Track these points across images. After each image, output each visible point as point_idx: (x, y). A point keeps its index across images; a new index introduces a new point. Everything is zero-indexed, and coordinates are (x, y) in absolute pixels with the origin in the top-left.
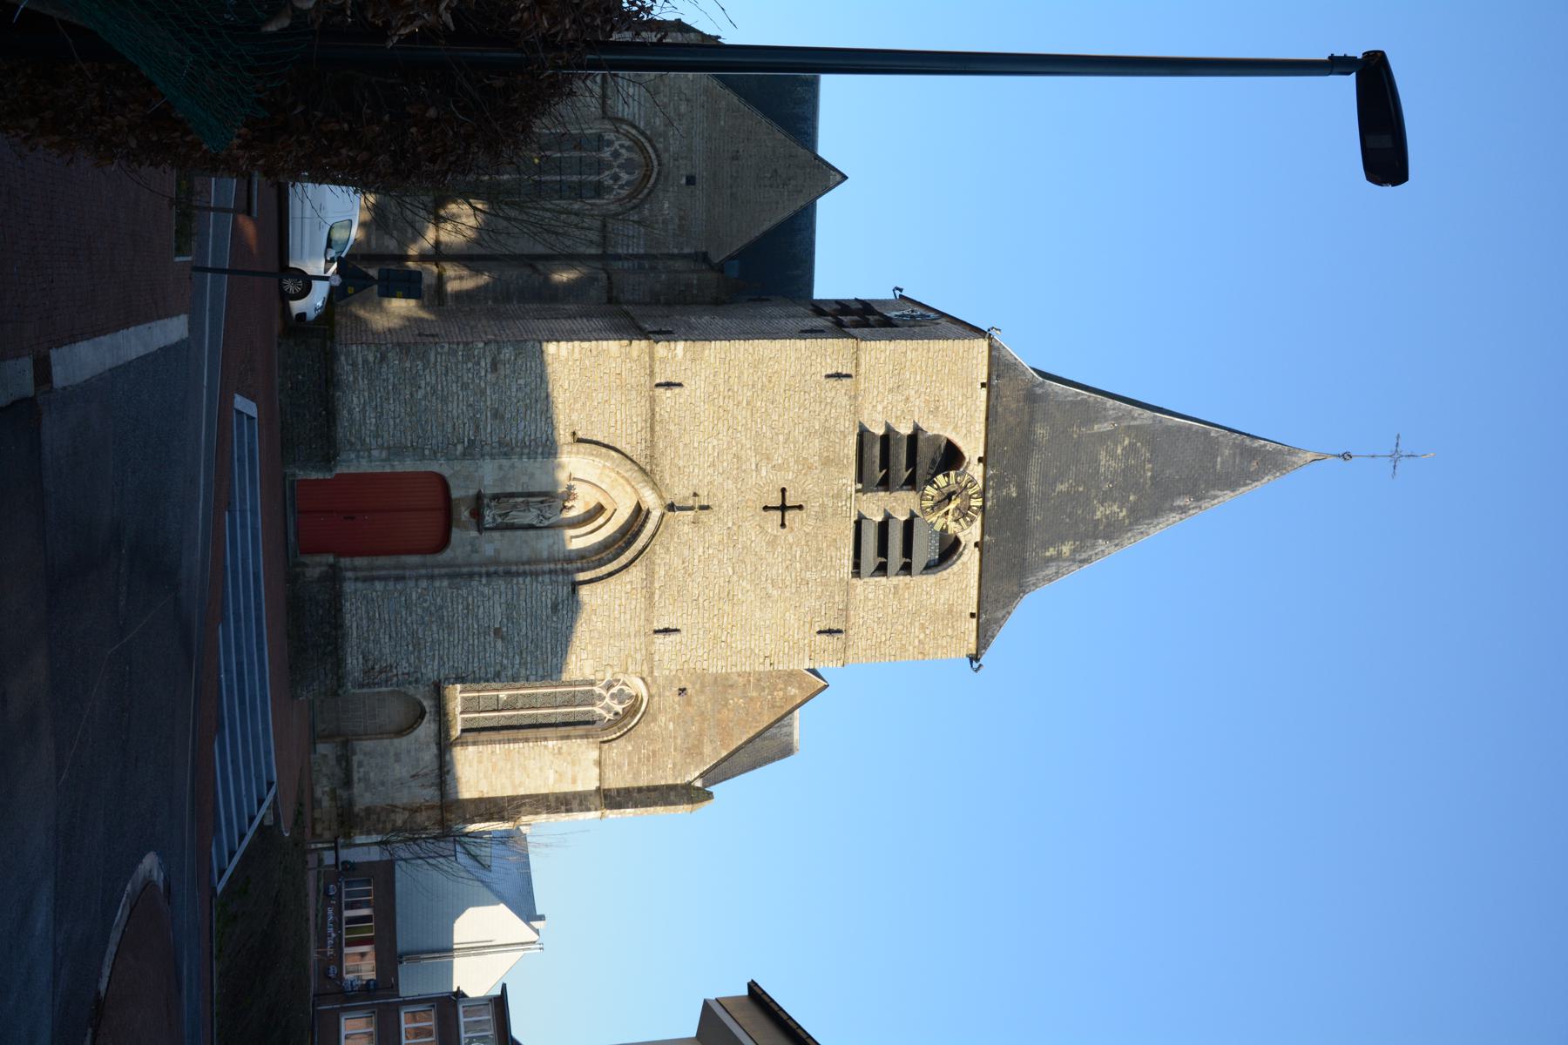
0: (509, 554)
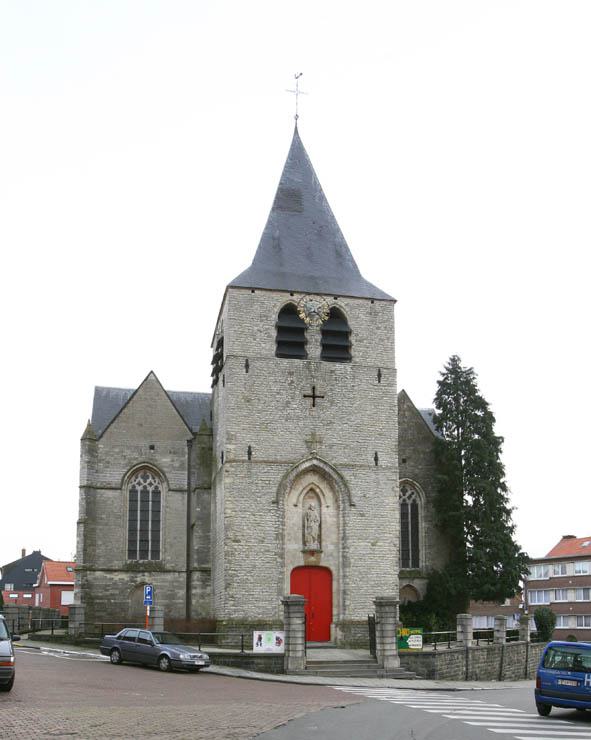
0: (334, 537)
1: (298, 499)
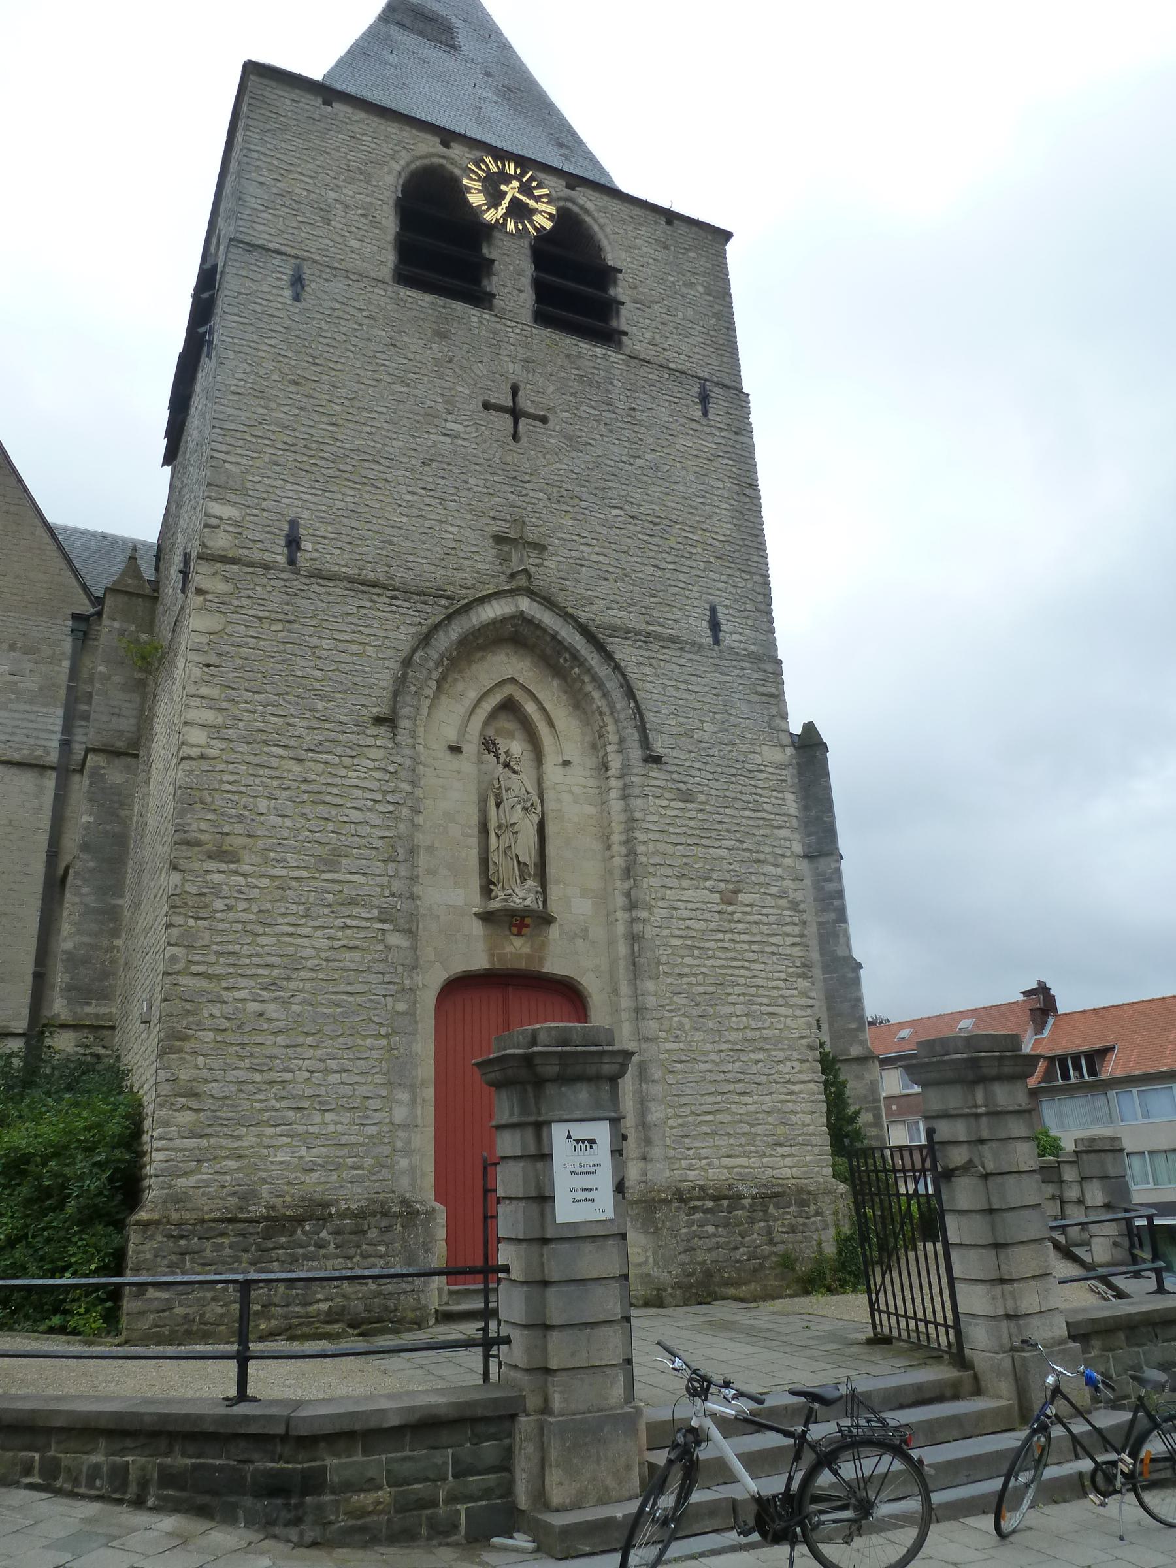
1: (463, 730)
